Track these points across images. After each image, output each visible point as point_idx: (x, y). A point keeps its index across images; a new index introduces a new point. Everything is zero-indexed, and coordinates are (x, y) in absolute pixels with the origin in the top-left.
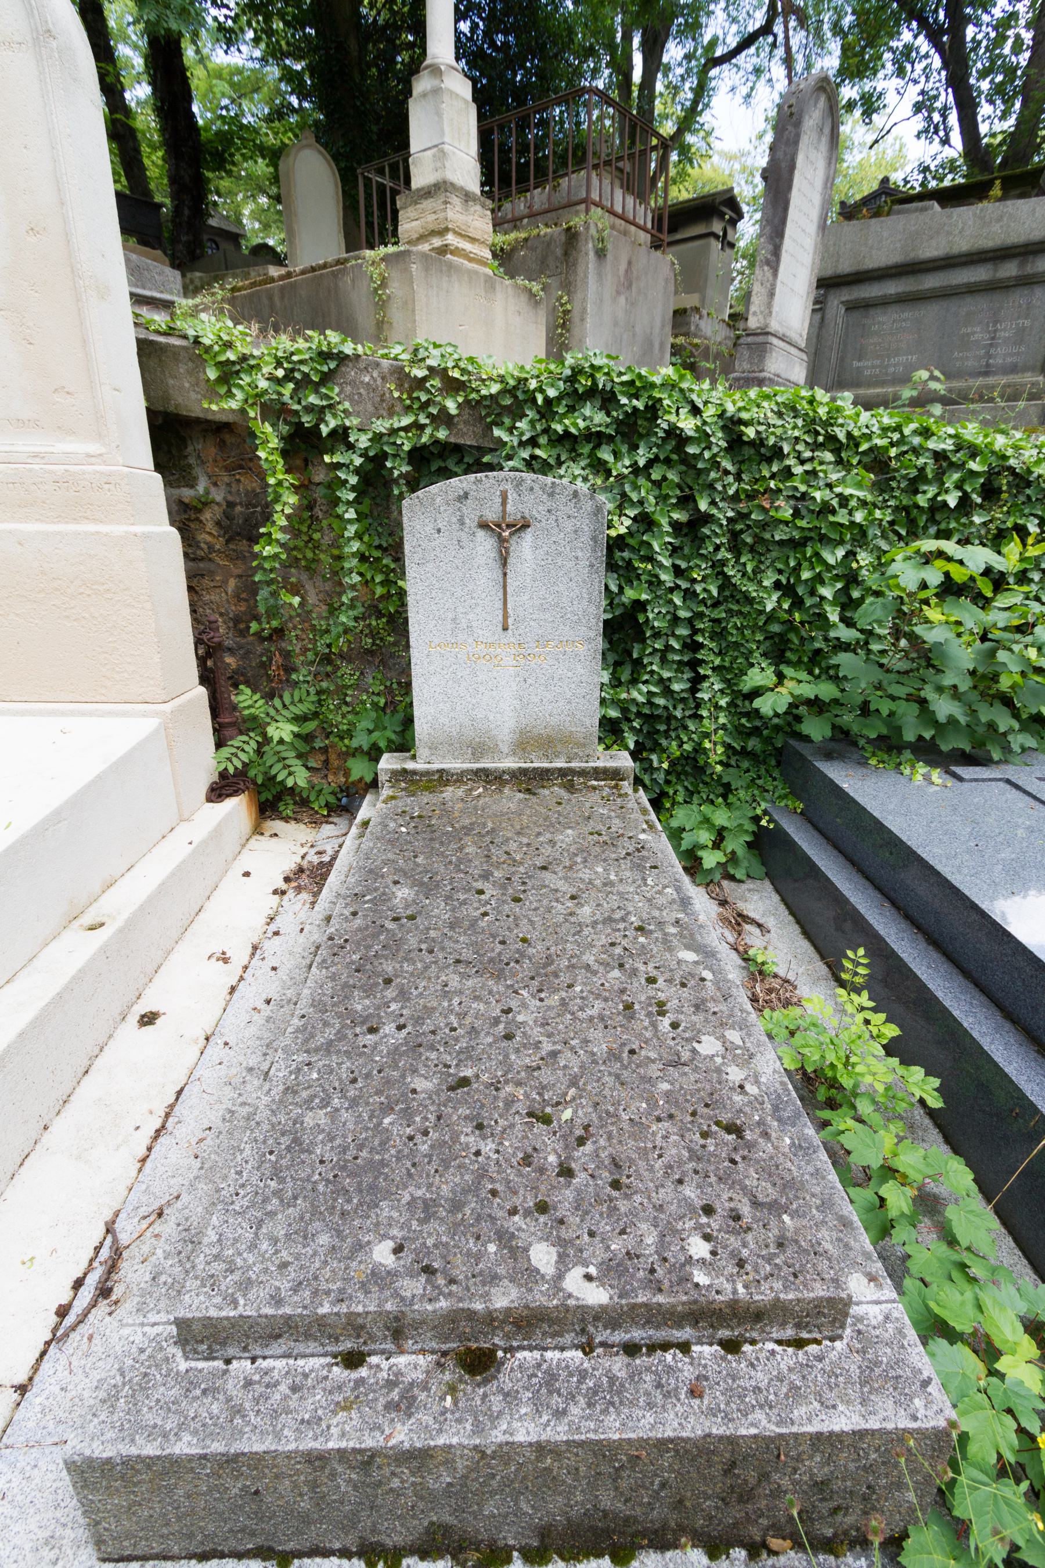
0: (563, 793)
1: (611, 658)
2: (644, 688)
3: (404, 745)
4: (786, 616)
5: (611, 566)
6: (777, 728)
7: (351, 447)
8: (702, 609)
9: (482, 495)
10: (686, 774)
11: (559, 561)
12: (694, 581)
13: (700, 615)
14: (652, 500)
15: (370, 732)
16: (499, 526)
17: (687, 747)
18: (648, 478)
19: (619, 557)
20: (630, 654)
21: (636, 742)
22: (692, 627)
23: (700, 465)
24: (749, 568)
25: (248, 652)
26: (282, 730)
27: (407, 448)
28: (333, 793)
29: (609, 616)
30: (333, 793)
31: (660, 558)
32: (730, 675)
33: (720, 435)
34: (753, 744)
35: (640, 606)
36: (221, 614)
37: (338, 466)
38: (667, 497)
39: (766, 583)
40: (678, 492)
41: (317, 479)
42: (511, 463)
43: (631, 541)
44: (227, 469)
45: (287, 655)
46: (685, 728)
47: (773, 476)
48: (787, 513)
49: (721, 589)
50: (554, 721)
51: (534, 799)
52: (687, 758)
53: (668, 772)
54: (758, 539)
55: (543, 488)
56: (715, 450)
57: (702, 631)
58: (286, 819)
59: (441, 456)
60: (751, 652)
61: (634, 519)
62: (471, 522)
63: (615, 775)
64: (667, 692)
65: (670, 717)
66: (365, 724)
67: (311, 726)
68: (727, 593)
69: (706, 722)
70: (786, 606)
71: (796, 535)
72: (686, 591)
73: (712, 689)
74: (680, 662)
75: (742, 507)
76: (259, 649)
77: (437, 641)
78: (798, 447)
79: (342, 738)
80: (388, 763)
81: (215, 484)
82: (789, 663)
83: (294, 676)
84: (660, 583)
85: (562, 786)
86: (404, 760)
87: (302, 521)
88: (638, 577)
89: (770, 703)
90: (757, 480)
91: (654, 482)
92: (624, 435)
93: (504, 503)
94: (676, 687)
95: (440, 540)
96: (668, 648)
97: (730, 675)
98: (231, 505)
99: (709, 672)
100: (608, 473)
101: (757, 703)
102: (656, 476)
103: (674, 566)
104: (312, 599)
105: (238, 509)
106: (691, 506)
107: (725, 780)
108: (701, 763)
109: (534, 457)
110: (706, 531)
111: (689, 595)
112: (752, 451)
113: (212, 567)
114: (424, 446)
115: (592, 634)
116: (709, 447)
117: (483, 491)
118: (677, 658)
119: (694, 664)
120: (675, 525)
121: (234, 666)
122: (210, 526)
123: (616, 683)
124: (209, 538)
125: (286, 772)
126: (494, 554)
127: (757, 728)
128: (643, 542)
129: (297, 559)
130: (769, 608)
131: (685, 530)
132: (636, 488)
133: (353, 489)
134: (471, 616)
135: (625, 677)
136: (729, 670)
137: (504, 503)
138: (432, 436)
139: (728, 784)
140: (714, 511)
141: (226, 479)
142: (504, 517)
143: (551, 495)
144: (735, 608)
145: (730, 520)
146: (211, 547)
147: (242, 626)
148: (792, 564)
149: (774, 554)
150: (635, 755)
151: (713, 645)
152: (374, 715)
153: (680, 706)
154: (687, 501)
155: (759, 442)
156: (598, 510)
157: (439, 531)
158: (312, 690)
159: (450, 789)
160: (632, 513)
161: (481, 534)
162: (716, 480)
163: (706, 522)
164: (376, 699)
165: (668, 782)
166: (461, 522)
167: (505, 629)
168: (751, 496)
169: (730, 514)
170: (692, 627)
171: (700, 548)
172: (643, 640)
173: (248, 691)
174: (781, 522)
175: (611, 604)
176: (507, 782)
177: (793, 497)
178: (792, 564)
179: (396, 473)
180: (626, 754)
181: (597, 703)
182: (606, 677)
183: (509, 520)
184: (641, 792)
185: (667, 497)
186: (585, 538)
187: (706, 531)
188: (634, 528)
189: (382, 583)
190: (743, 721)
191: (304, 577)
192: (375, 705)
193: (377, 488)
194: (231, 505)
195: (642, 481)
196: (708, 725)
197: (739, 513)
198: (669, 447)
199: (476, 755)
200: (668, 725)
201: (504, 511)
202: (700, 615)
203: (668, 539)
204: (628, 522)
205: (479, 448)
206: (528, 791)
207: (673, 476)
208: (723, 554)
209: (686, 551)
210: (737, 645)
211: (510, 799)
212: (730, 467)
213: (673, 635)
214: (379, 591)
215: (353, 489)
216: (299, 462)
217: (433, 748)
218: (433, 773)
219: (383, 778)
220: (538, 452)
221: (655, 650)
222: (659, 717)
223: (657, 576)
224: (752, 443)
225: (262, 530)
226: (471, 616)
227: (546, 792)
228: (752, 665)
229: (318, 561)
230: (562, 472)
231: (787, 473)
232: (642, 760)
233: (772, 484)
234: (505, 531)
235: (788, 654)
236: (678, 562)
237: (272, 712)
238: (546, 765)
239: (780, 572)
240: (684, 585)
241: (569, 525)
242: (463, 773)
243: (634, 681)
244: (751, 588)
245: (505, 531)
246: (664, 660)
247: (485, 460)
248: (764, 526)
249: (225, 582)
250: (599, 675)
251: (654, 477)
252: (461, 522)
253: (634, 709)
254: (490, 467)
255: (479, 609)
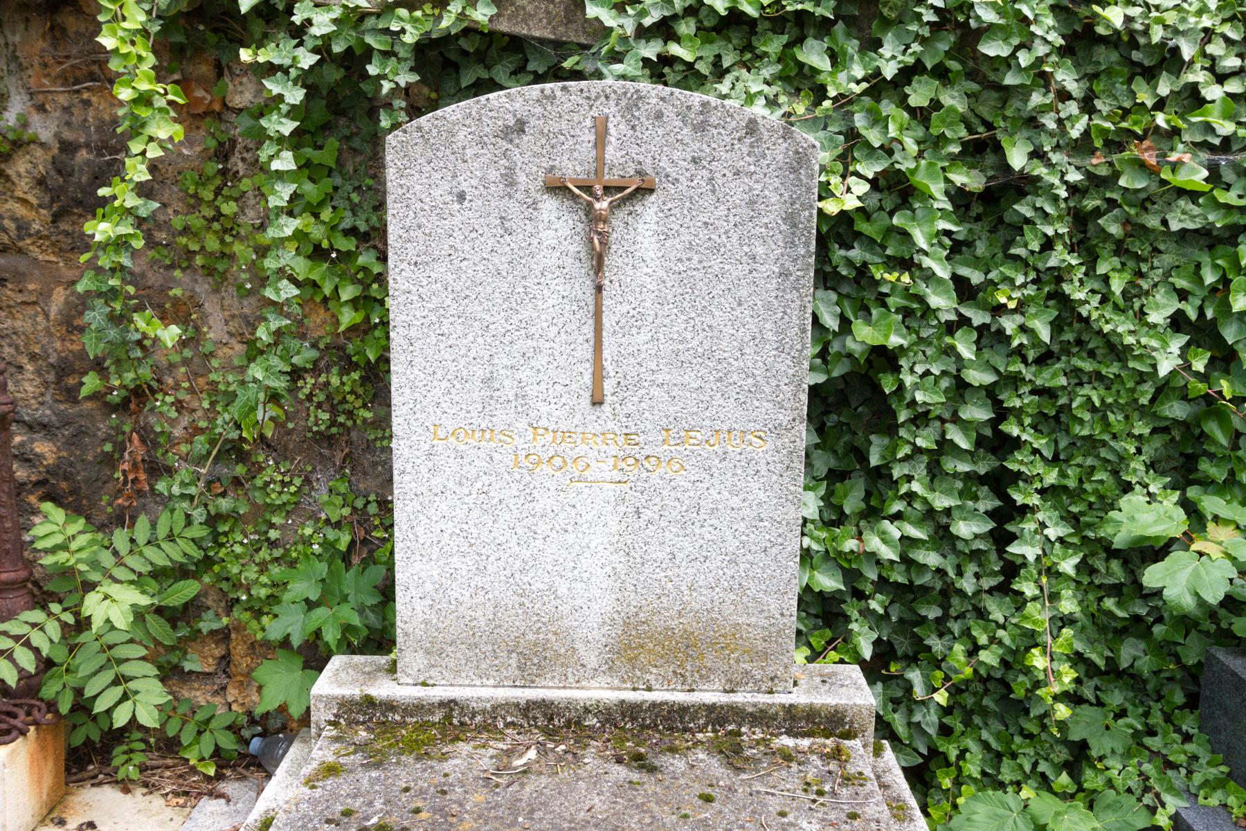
0: (714, 766)
1: (823, 464)
2: (894, 531)
3: (378, 640)
4: (1202, 387)
5: (826, 278)
6: (1186, 623)
7: (299, 33)
8: (1017, 367)
9: (554, 126)
10: (985, 713)
11: (715, 264)
12: (999, 310)
13: (1014, 381)
14: (912, 147)
15: (310, 605)
16: (588, 189)
17: (989, 657)
18: (903, 102)
19: (844, 257)
20: (863, 458)
21: (877, 643)
22: (997, 404)
23: (1010, 80)
24: (1117, 285)
25: (80, 433)
26: (113, 606)
27: (410, 38)
28: (233, 728)
29: (821, 378)
30: (233, 728)
31: (927, 262)
32: (1083, 509)
33: (1050, 21)
34: (1130, 652)
35: (885, 358)
36: (33, 357)
37: (271, 69)
38: (941, 141)
39: (1155, 317)
40: (963, 133)
41: (238, 101)
42: (618, 68)
43: (862, 226)
44: (64, 79)
45: (148, 438)
46: (982, 614)
47: (1160, 105)
48: (1195, 175)
49: (1057, 327)
50: (698, 601)
51: (650, 784)
52: (985, 680)
53: (947, 711)
54: (1136, 229)
55: (683, 114)
56: (1041, 50)
57: (1018, 413)
58: (125, 786)
59: (481, 58)
60: (1123, 458)
61: (874, 183)
62: (529, 179)
63: (834, 724)
64: (943, 537)
65: (948, 592)
66: (302, 587)
67: (186, 590)
68: (1069, 336)
69: (1031, 608)
70: (1199, 365)
71: (1217, 220)
72: (983, 329)
73: (1040, 536)
74: (968, 477)
75: (1098, 164)
76: (103, 428)
77: (450, 425)
78: (1210, 49)
79: (258, 614)
80: (338, 680)
81: (41, 108)
82: (1207, 483)
83: (161, 486)
84: (928, 312)
85: (716, 748)
86: (371, 676)
87: (203, 181)
88: (882, 300)
89: (1183, 577)
90: (1126, 113)
91: (912, 111)
92: (850, 22)
93: (600, 142)
94: (964, 529)
95: (460, 216)
96: (945, 445)
97: (1083, 509)
98: (68, 148)
99: (1035, 500)
100: (820, 93)
101: (1152, 576)
102: (918, 96)
103: (956, 278)
104: (215, 331)
105: (83, 155)
106: (990, 159)
107: (1075, 736)
108: (1019, 693)
109: (667, 60)
110: (1024, 209)
111: (990, 337)
112: (1114, 56)
113: (22, 264)
114: (447, 39)
115: (784, 418)
116: (1026, 46)
117: (555, 120)
118: (963, 467)
119: (1000, 481)
120: (959, 197)
121: (50, 460)
122: (23, 187)
123: (834, 518)
124: (21, 211)
125: (118, 692)
126: (575, 247)
127: (1137, 618)
128: (891, 230)
129: (191, 254)
130: (1163, 370)
131: (977, 209)
132: (879, 121)
133: (293, 112)
134: (523, 375)
135: (852, 503)
136: (1077, 494)
137: (600, 142)
138: (462, 16)
139: (1083, 745)
140: (1040, 170)
141: (63, 100)
142: (598, 172)
143: (701, 128)
144: (1087, 366)
145: (1073, 189)
146: (23, 227)
147: (71, 381)
148: (1210, 278)
149: (1167, 259)
150: (874, 671)
151: (1040, 443)
152: (322, 568)
153: (971, 568)
154: (982, 149)
155: (1126, 40)
156: (800, 159)
157: (461, 197)
158: (199, 515)
159: (464, 748)
160: (870, 169)
161: (550, 206)
162: (1044, 109)
163: (1021, 194)
164: (331, 534)
165: (946, 731)
166: (509, 180)
167: (597, 402)
168: (1114, 144)
169: (1074, 177)
170: (997, 404)
171: (1009, 243)
172: (891, 429)
173: (58, 514)
174: (1181, 192)
175: (823, 354)
176: (592, 734)
177: (1205, 145)
178: (1210, 278)
179: (386, 86)
180: (855, 672)
181: (794, 564)
182: (811, 505)
183: (611, 177)
184: (889, 754)
185: (941, 141)
186: (773, 216)
187: (1024, 209)
188: (873, 201)
189: (354, 303)
190: (1109, 603)
191: (202, 287)
192: (327, 545)
193: (345, 114)
194: (68, 148)
195: (887, 107)
196: (1038, 615)
197: (1090, 176)
198: (943, 47)
199: (527, 677)
200: (946, 607)
201: (600, 160)
202: (1014, 381)
203: (943, 225)
204: (863, 188)
205: (558, 44)
206: (638, 761)
207: (953, 100)
208: (1060, 257)
209: (981, 248)
210: (1092, 444)
211: (595, 780)
212: (1072, 86)
213: (956, 419)
214: (348, 317)
215: (293, 112)
216: (205, 69)
217: (434, 651)
218: (430, 708)
219: (320, 715)
220: (675, 49)
221: (918, 450)
222: (925, 589)
223: (921, 299)
224: (1113, 41)
225: (103, 192)
226: (523, 375)
227: (678, 764)
228: (1127, 488)
229: (232, 257)
230: (724, 87)
231: (1193, 98)
232: (887, 680)
233: (1161, 119)
234: (602, 200)
235: (1205, 466)
236: (964, 271)
237: (107, 559)
238: (680, 697)
239: (1183, 295)
240: (979, 318)
241: (737, 191)
242: (497, 709)
243: (872, 513)
244: (1122, 326)
245: (602, 200)
246: (935, 472)
247: (567, 64)
248: (1145, 202)
249: (46, 294)
250: (800, 504)
251: (913, 101)
252: (509, 180)
253: (872, 575)
254: (577, 75)
255: (543, 360)
